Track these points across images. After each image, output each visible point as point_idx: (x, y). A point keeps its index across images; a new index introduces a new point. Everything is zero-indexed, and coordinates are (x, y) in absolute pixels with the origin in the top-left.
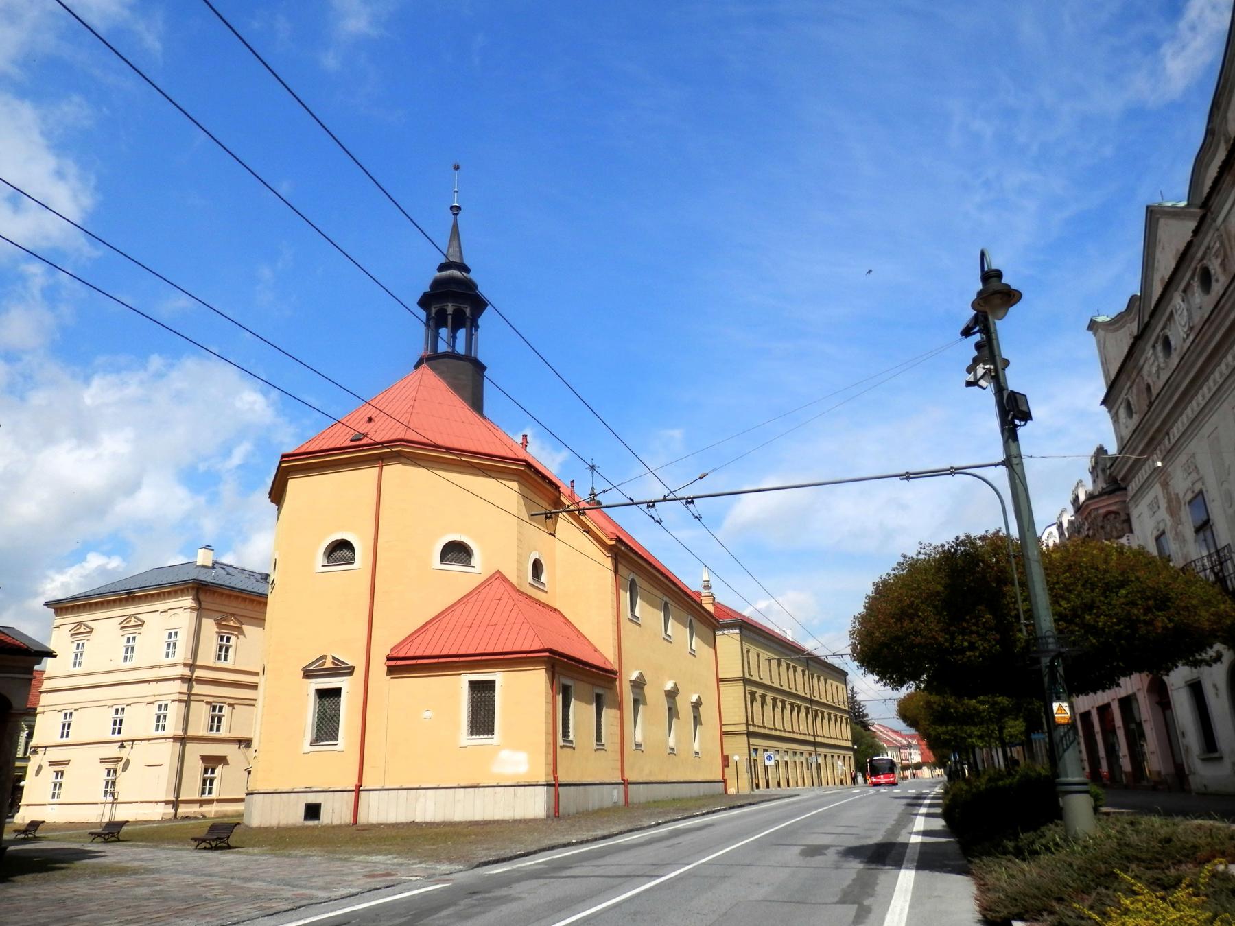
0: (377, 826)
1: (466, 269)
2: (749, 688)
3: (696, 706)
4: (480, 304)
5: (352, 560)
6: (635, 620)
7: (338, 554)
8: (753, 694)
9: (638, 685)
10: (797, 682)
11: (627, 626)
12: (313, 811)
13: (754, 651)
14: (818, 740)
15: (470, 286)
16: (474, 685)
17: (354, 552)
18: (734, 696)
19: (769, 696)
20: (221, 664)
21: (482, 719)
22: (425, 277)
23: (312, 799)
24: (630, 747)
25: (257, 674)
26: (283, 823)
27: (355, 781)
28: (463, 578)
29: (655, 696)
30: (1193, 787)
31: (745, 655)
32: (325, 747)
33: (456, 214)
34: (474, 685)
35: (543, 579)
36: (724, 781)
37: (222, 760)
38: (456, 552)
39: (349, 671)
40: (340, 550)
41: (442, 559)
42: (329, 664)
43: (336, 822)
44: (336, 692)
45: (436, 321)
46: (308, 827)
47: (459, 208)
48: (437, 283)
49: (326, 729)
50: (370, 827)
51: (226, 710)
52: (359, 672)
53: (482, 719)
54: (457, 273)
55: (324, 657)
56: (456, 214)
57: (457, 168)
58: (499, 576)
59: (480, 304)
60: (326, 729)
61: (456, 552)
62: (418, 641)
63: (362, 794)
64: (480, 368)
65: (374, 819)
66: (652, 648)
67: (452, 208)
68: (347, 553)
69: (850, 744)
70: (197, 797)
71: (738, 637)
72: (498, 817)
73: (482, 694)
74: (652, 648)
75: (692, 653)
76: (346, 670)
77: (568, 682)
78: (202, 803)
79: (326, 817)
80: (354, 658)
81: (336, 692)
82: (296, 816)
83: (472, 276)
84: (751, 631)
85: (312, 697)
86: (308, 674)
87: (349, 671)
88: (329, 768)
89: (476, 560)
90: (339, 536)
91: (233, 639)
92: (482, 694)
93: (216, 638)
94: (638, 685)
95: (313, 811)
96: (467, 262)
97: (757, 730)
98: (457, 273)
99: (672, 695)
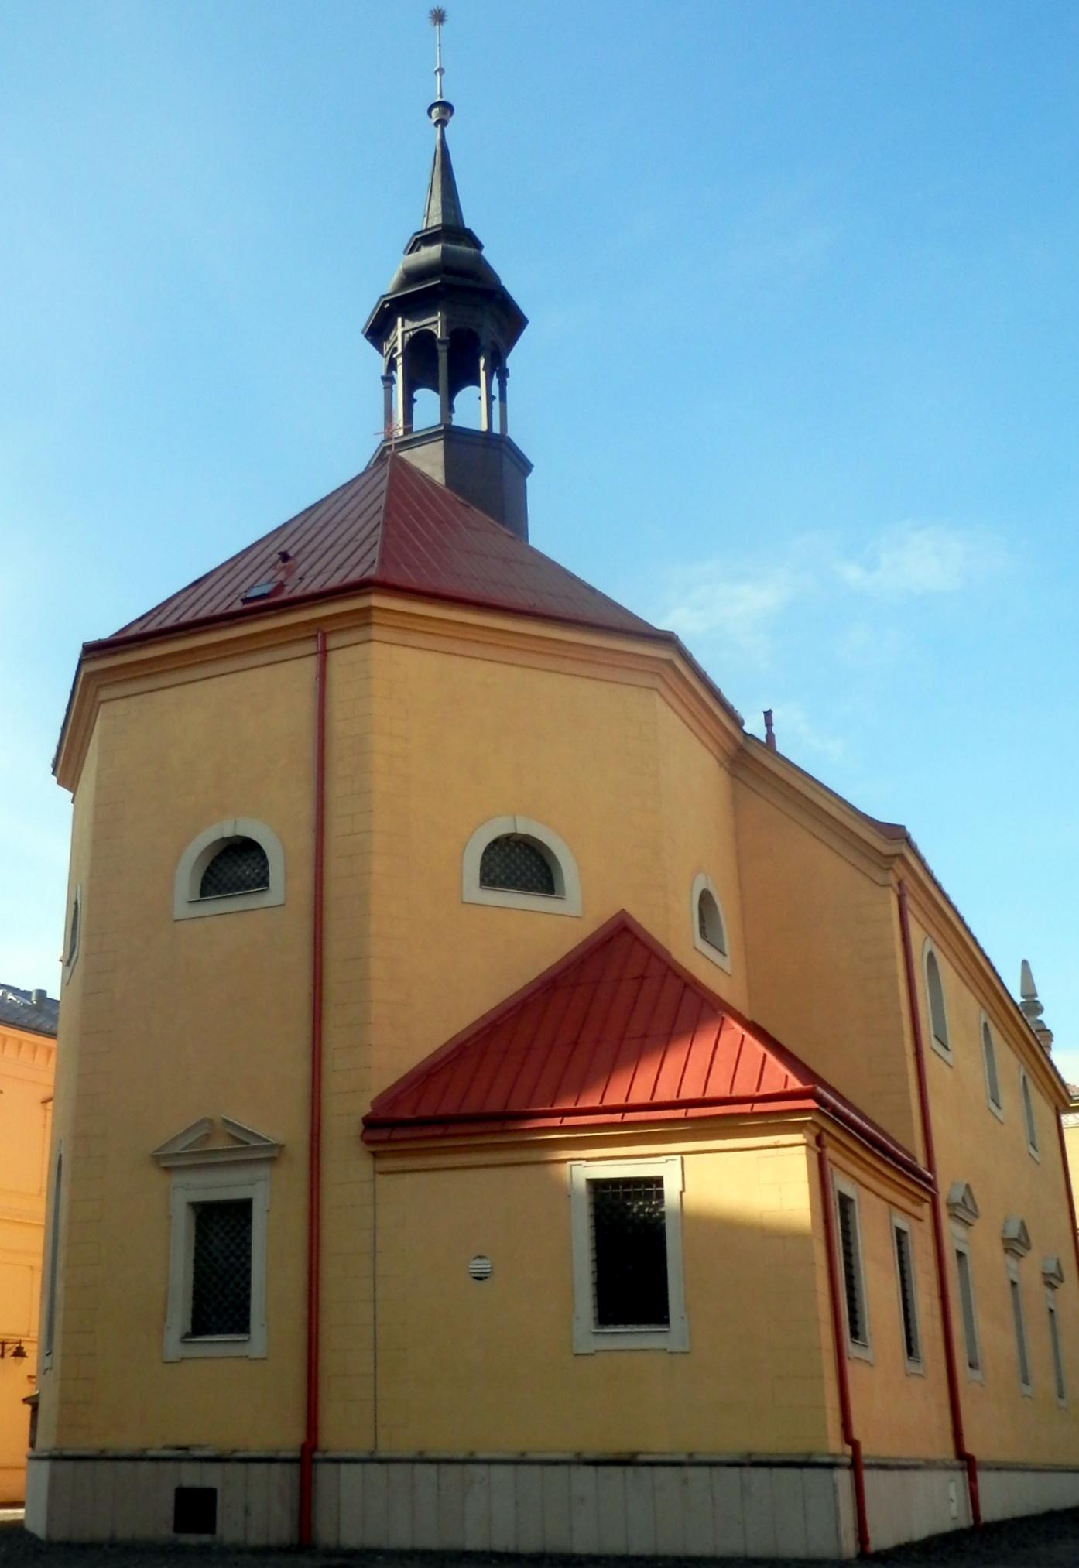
23: (193, 1476)
32: (217, 1346)
33: (442, 123)
39: (271, 1155)
65: (351, 1538)
68: (246, 870)
79: (229, 1527)
95: (196, 1507)
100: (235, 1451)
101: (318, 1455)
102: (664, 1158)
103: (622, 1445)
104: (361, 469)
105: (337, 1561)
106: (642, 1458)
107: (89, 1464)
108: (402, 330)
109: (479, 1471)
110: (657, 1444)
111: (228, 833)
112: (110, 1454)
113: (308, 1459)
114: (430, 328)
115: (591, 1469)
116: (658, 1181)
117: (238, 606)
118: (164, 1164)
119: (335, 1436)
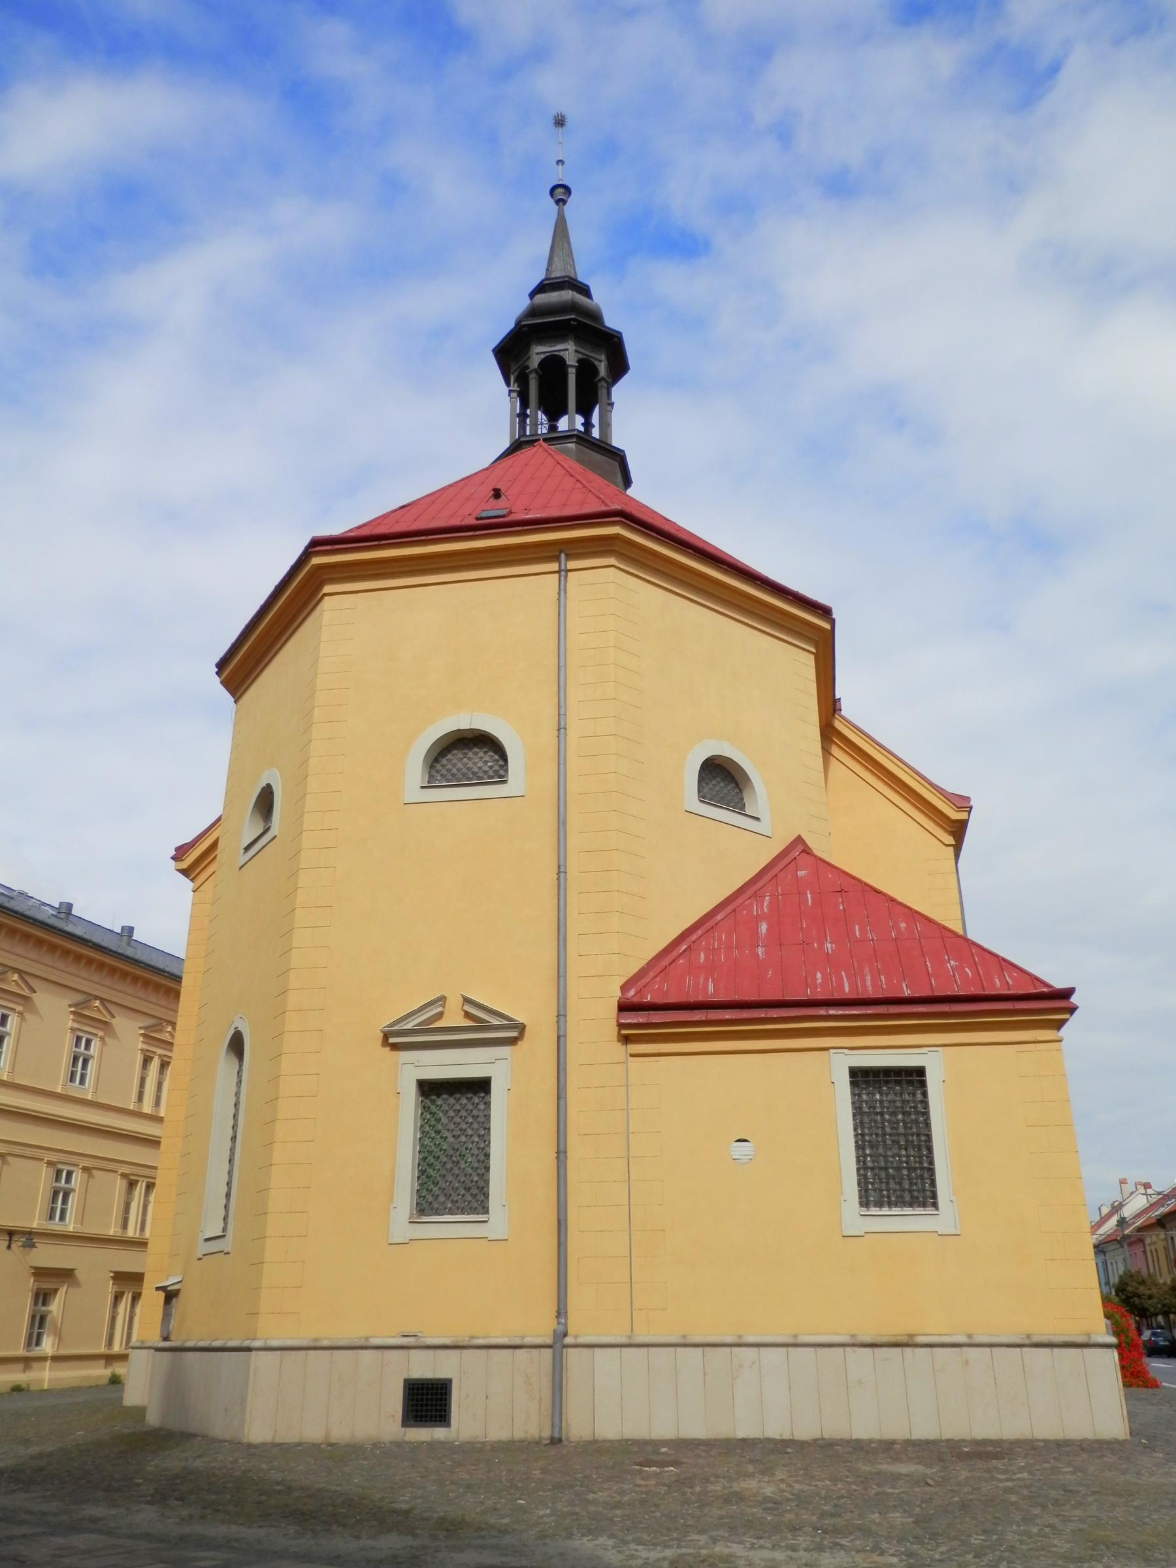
0: (641, 1453)
1: (585, 291)
5: (499, 775)
7: (458, 760)
12: (427, 1401)
17: (503, 756)
20: (75, 1090)
22: (507, 307)
23: (425, 1368)
26: (340, 1433)
32: (449, 1229)
33: (561, 202)
37: (66, 1275)
39: (512, 1034)
40: (467, 754)
42: (454, 1017)
43: (498, 1432)
46: (416, 1446)
48: (533, 312)
49: (452, 1177)
50: (596, 1448)
51: (78, 1178)
52: (539, 1043)
54: (567, 295)
55: (443, 999)
56: (561, 202)
60: (452, 1177)
63: (573, 1357)
65: (610, 1428)
68: (480, 759)
70: (21, 1352)
72: (1046, 1429)
76: (495, 1030)
78: (27, 1362)
79: (467, 1420)
80: (525, 1003)
82: (379, 1416)
85: (410, 1094)
87: (512, 1034)
88: (457, 1290)
91: (95, 1045)
93: (69, 1038)
95: (427, 1401)
98: (567, 295)
100: (472, 1338)
101: (568, 1340)
102: (925, 1050)
103: (896, 1328)
104: (487, 465)
105: (391, 1543)
106: (920, 1339)
107: (303, 1352)
108: (538, 353)
109: (748, 1354)
110: (933, 1327)
111: (464, 725)
112: (325, 1343)
113: (559, 1343)
114: (561, 354)
115: (868, 1350)
116: (920, 1072)
117: (473, 522)
118: (467, 1008)
119: (581, 1327)
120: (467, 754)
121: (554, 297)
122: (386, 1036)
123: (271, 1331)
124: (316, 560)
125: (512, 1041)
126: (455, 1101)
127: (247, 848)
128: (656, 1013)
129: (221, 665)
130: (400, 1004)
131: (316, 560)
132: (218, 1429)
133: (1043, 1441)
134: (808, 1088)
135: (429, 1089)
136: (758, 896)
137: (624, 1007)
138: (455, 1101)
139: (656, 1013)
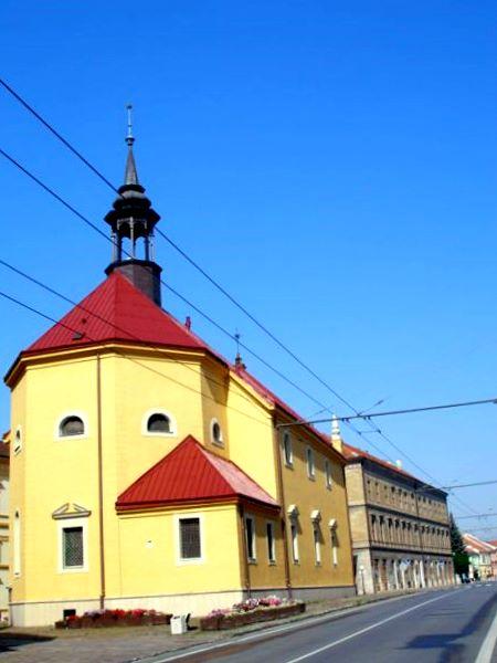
1: (140, 189)
2: (371, 512)
3: (334, 529)
4: (154, 218)
5: (81, 431)
6: (289, 466)
8: (374, 517)
9: (295, 515)
10: (406, 504)
11: (284, 470)
13: (373, 479)
14: (426, 550)
15: (146, 202)
16: (184, 522)
18: (358, 519)
19: (387, 517)
21: (191, 542)
23: (68, 607)
24: (292, 562)
25: (6, 517)
27: (100, 593)
28: (164, 444)
29: (306, 524)
30: (234, 507)
31: (366, 483)
32: (74, 570)
34: (184, 522)
35: (221, 439)
36: (355, 586)
38: (158, 422)
40: (71, 424)
41: (149, 428)
42: (72, 510)
44: (79, 530)
45: (122, 232)
47: (132, 140)
48: (117, 204)
49: (73, 555)
52: (96, 515)
53: (191, 542)
54: (136, 194)
55: (68, 505)
57: (130, 107)
58: (190, 440)
59: (154, 218)
60: (73, 555)
61: (158, 422)
62: (136, 492)
64: (156, 270)
66: (309, 493)
67: (127, 140)
68: (75, 425)
69: (449, 552)
71: (360, 471)
73: (190, 530)
74: (309, 493)
75: (329, 488)
77: (251, 517)
80: (93, 506)
81: (79, 530)
83: (146, 195)
84: (370, 465)
85: (60, 534)
86: (56, 517)
87: (89, 514)
89: (173, 426)
90: (71, 414)
92: (190, 530)
94: (295, 515)
96: (141, 183)
97: (377, 544)
98: (136, 194)
99: (317, 522)
120: (71, 424)
121: (127, 194)
122: (53, 516)
123: (29, 599)
124: (23, 360)
125: (88, 516)
126: (73, 534)
127: (74, 339)
128: (130, 503)
129: (5, 380)
130: (56, 506)
131: (23, 360)
132: (20, 625)
133: (209, 630)
134: (166, 524)
135: (67, 531)
136: (142, 483)
137: (117, 504)
138: (73, 534)
139: (130, 503)
